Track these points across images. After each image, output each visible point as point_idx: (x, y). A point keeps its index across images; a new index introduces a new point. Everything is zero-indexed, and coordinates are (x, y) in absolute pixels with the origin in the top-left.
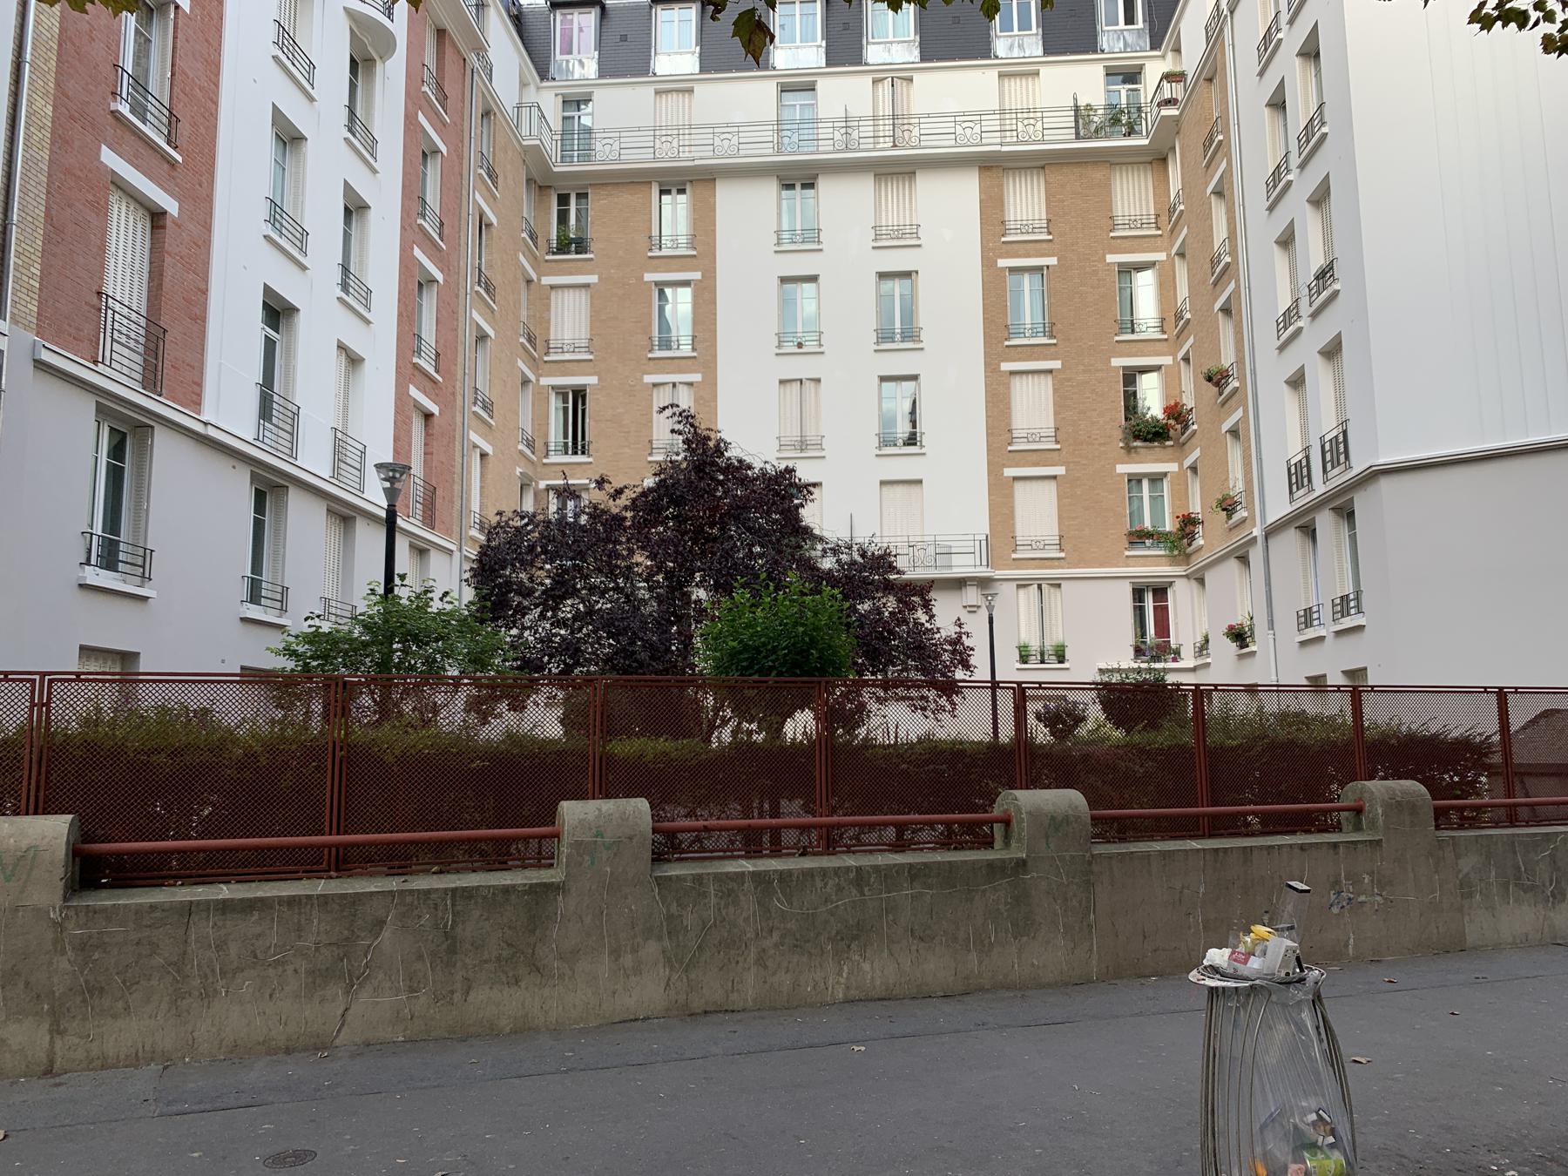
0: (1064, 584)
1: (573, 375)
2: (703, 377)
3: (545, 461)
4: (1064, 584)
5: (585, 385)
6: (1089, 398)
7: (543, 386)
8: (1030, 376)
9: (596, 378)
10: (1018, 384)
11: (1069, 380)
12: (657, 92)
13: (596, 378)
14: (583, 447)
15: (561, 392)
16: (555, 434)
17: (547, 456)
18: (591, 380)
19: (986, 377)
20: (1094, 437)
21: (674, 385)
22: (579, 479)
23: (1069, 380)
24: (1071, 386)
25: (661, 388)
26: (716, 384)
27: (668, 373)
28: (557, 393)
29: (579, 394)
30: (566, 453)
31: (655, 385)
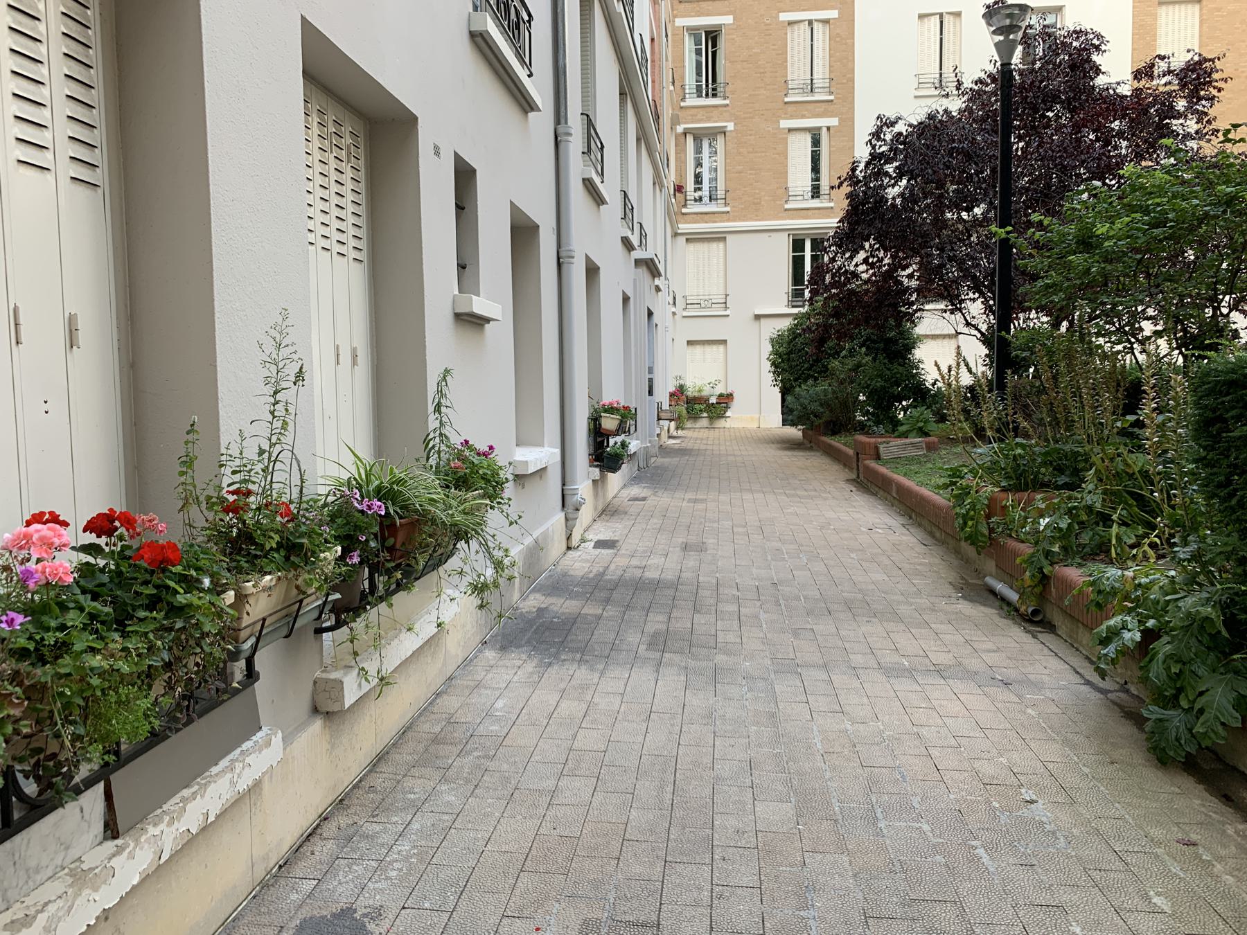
0: (729, 237)
1: (708, 15)
2: (839, 14)
3: (684, 210)
4: (729, 237)
5: (720, 25)
6: (1238, 28)
7: (678, 27)
8: (1177, 6)
9: (731, 17)
10: (1164, 14)
11: (1218, 10)
12: (687, 240)
13: (731, 17)
14: (714, 89)
15: (693, 31)
16: (690, 79)
17: (683, 99)
18: (728, 20)
19: (1134, 7)
20: (1240, 70)
21: (810, 22)
22: (716, 122)
23: (1218, 10)
24: (1222, 16)
25: (796, 27)
26: (853, 20)
27: (804, 10)
28: (690, 34)
29: (713, 36)
30: (700, 96)
31: (790, 23)
